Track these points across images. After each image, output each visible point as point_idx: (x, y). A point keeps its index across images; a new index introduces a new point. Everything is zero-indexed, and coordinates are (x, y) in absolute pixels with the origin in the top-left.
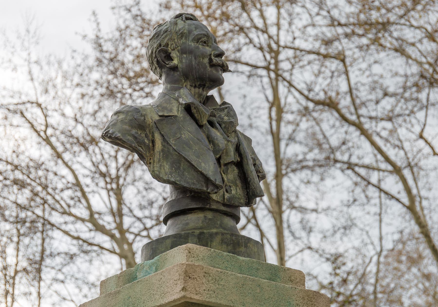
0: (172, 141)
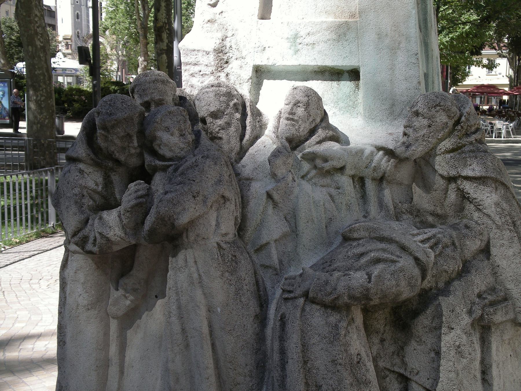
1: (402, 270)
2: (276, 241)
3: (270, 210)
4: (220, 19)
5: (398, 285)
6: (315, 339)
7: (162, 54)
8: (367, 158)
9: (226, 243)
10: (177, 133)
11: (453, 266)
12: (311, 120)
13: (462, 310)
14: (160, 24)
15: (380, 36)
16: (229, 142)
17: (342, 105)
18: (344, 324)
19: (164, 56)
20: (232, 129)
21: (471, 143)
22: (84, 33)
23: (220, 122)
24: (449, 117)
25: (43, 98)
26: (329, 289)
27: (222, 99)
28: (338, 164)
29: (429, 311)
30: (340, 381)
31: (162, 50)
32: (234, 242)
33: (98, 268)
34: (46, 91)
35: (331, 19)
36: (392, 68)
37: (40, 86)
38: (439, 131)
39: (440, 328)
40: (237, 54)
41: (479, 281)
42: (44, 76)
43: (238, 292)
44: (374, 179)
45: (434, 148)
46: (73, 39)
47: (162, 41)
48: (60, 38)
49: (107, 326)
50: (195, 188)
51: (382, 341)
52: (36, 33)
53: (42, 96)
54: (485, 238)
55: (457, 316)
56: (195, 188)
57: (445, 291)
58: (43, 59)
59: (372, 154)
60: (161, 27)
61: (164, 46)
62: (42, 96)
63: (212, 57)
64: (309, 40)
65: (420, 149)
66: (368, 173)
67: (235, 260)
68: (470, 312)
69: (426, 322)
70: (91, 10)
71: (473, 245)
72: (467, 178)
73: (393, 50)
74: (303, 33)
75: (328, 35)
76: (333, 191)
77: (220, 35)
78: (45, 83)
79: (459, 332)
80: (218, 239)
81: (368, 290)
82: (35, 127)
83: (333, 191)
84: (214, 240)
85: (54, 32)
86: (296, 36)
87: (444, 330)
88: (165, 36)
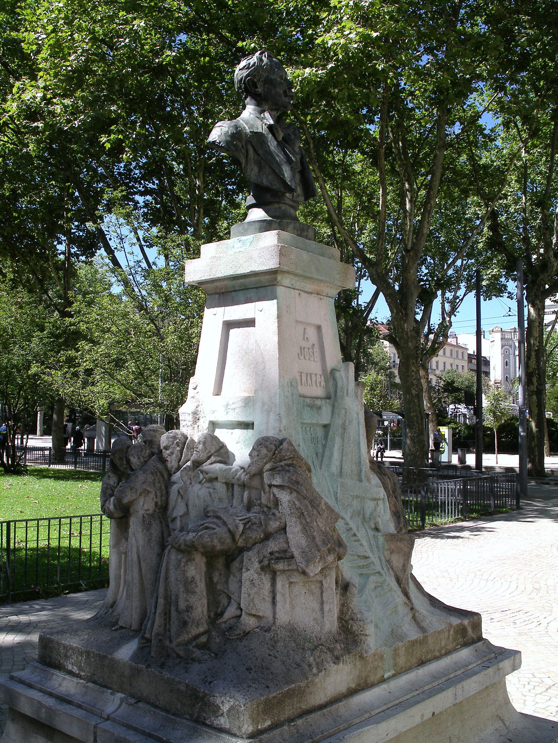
0: (260, 152)
1: (215, 533)
2: (181, 516)
3: (180, 500)
4: (197, 396)
5: (212, 541)
6: (171, 567)
7: (532, 395)
8: (233, 473)
9: (147, 514)
10: (136, 457)
11: (257, 535)
12: (207, 451)
13: (255, 560)
14: (531, 370)
15: (263, 404)
16: (171, 462)
17: (247, 443)
18: (184, 560)
19: (535, 397)
20: (174, 456)
21: (281, 466)
22: (512, 376)
23: (168, 452)
24: (268, 451)
25: (416, 435)
26: (177, 540)
27: (171, 439)
28: (214, 476)
29: (238, 559)
30: (179, 590)
31: (533, 391)
32: (152, 515)
33: (118, 527)
34: (419, 429)
35: (246, 395)
36: (267, 423)
37: (414, 425)
38: (264, 459)
39: (241, 569)
40: (203, 415)
41: (273, 546)
42: (418, 417)
43: (149, 540)
44: (239, 485)
45: (262, 468)
46: (502, 382)
47: (532, 384)
48: (492, 383)
49: (121, 557)
50: (132, 485)
51: (220, 574)
52: (413, 384)
53: (415, 433)
54: (283, 521)
55: (252, 563)
56: (132, 485)
57: (249, 549)
58: (417, 404)
59: (237, 470)
60: (532, 373)
61: (534, 388)
62: (415, 433)
63: (191, 416)
64: (233, 406)
65: (254, 468)
66: (234, 481)
67: (150, 524)
68: (260, 562)
69: (237, 565)
70: (517, 358)
71: (274, 525)
72: (275, 486)
73: (269, 412)
74: (230, 403)
75: (241, 404)
76: (211, 490)
77: (195, 405)
78: (418, 423)
79: (252, 572)
80: (143, 512)
81: (193, 542)
82: (409, 458)
83: (211, 490)
84: (141, 512)
85: (487, 378)
86: (228, 405)
87: (244, 570)
88: (535, 380)
